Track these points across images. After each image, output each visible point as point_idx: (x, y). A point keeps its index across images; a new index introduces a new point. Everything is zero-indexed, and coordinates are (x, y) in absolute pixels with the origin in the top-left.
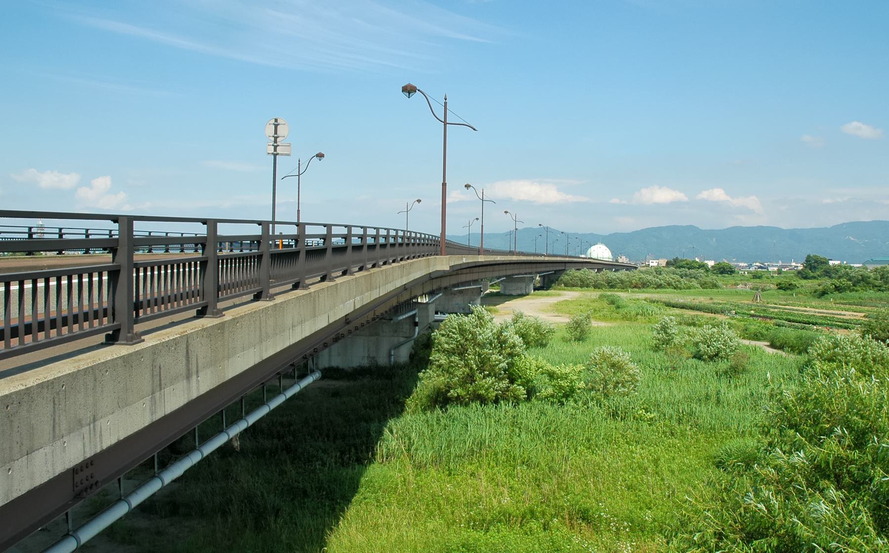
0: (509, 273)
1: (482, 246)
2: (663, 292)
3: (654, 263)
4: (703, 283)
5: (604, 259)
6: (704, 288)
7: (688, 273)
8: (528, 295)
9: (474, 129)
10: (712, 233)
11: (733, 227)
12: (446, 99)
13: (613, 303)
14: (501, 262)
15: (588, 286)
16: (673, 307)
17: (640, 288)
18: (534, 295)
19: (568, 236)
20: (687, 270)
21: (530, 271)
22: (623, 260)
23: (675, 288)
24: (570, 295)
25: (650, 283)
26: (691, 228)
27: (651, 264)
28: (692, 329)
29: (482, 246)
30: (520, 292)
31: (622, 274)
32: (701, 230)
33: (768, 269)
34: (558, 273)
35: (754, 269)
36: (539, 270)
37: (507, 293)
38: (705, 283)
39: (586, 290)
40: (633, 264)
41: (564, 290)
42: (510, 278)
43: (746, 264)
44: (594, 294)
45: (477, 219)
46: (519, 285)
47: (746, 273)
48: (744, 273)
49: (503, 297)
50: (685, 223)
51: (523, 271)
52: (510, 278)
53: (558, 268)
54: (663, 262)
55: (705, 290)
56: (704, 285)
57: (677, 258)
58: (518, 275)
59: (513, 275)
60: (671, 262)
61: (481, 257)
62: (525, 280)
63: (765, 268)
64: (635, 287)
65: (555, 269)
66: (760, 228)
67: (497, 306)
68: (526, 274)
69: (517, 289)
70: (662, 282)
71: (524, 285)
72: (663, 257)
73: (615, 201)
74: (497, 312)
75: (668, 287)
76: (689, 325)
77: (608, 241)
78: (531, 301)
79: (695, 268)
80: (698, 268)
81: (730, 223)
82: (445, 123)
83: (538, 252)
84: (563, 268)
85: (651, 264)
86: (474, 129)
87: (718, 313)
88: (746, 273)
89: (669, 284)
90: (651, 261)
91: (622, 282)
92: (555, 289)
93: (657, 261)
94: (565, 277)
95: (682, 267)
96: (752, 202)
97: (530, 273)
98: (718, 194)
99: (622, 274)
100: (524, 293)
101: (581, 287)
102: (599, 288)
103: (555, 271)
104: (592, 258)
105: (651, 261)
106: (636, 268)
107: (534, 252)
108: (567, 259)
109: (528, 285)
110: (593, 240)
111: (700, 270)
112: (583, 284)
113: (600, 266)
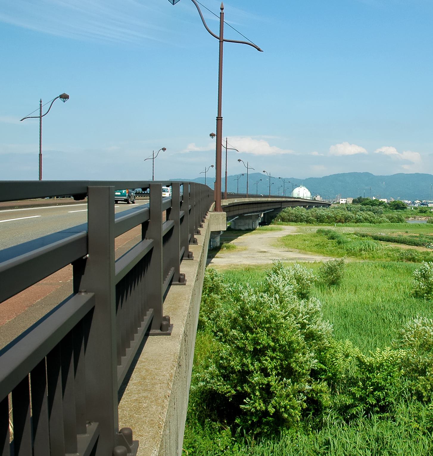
0: (241, 212)
1: (153, 180)
2: (362, 226)
3: (343, 201)
4: (391, 218)
5: (308, 199)
6: (392, 222)
7: (371, 209)
8: (254, 229)
9: (259, 50)
10: (382, 179)
11: (397, 174)
12: (222, 9)
13: (332, 238)
14: (242, 203)
15: (301, 221)
16: (380, 240)
17: (343, 222)
18: (260, 230)
19: (284, 181)
20: (371, 206)
21: (255, 210)
22: (318, 198)
23: (370, 223)
24: (289, 229)
25: (351, 218)
26: (367, 174)
27: (341, 202)
28: (412, 264)
29: (153, 180)
30: (247, 228)
31: (321, 211)
32: (375, 176)
33: (428, 206)
34: (279, 210)
35: (418, 206)
36: (263, 209)
37: (237, 228)
38: (392, 218)
39: (299, 225)
40: (327, 202)
41: (282, 224)
42: (241, 216)
43: (410, 202)
44: (315, 228)
45: (212, 166)
46: (247, 221)
47: (413, 208)
48: (411, 208)
49: (234, 232)
50: (362, 171)
51: (251, 210)
52: (241, 216)
53: (276, 207)
54: (350, 200)
55: (392, 224)
56: (392, 220)
57: (361, 197)
58: (248, 213)
59: (244, 214)
60: (356, 200)
61: (225, 201)
62: (252, 217)
63: (426, 205)
64: (339, 222)
65: (274, 207)
66: (418, 175)
67: (232, 242)
68: (253, 212)
69: (245, 225)
70: (361, 217)
71: (251, 221)
72: (349, 197)
73: (315, 153)
74: (235, 248)
75: (365, 221)
76: (409, 260)
77: (308, 183)
78: (259, 236)
79: (376, 205)
80: (379, 205)
81: (396, 171)
82: (221, 41)
83: (272, 194)
84: (280, 206)
85: (341, 202)
86: (259, 50)
87: (420, 245)
88: (413, 208)
89: (366, 219)
90: (341, 199)
91: (329, 217)
92: (275, 224)
93: (346, 199)
94: (283, 214)
95: (367, 204)
96: (408, 155)
97: (256, 212)
98: (390, 150)
99: (321, 211)
100: (251, 228)
101: (296, 221)
102: (310, 223)
103: (274, 209)
104: (300, 198)
105: (341, 199)
106: (330, 205)
107: (245, 192)
108: (284, 199)
109: (254, 221)
110: (296, 184)
111: (380, 207)
112: (297, 220)
113: (308, 204)
